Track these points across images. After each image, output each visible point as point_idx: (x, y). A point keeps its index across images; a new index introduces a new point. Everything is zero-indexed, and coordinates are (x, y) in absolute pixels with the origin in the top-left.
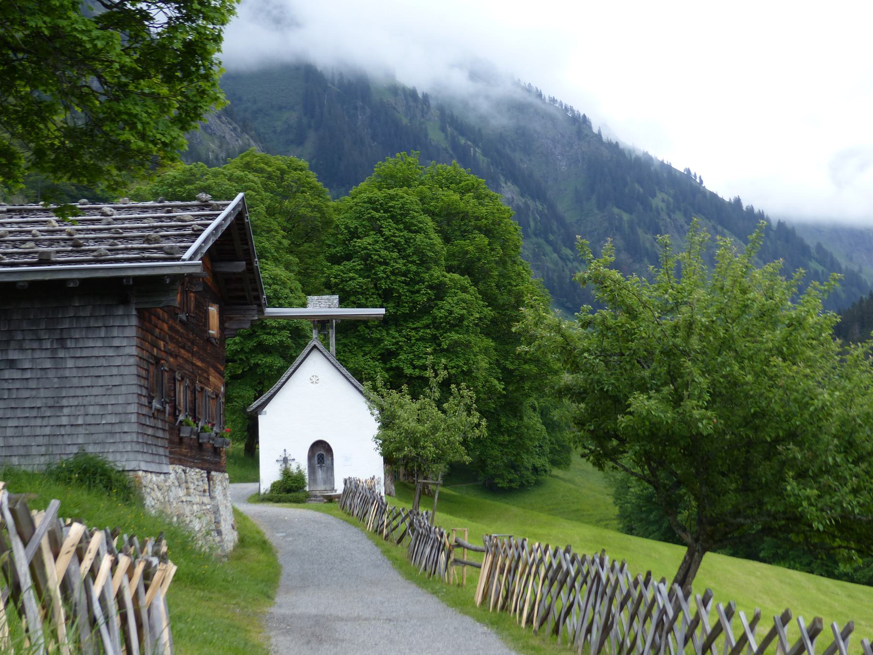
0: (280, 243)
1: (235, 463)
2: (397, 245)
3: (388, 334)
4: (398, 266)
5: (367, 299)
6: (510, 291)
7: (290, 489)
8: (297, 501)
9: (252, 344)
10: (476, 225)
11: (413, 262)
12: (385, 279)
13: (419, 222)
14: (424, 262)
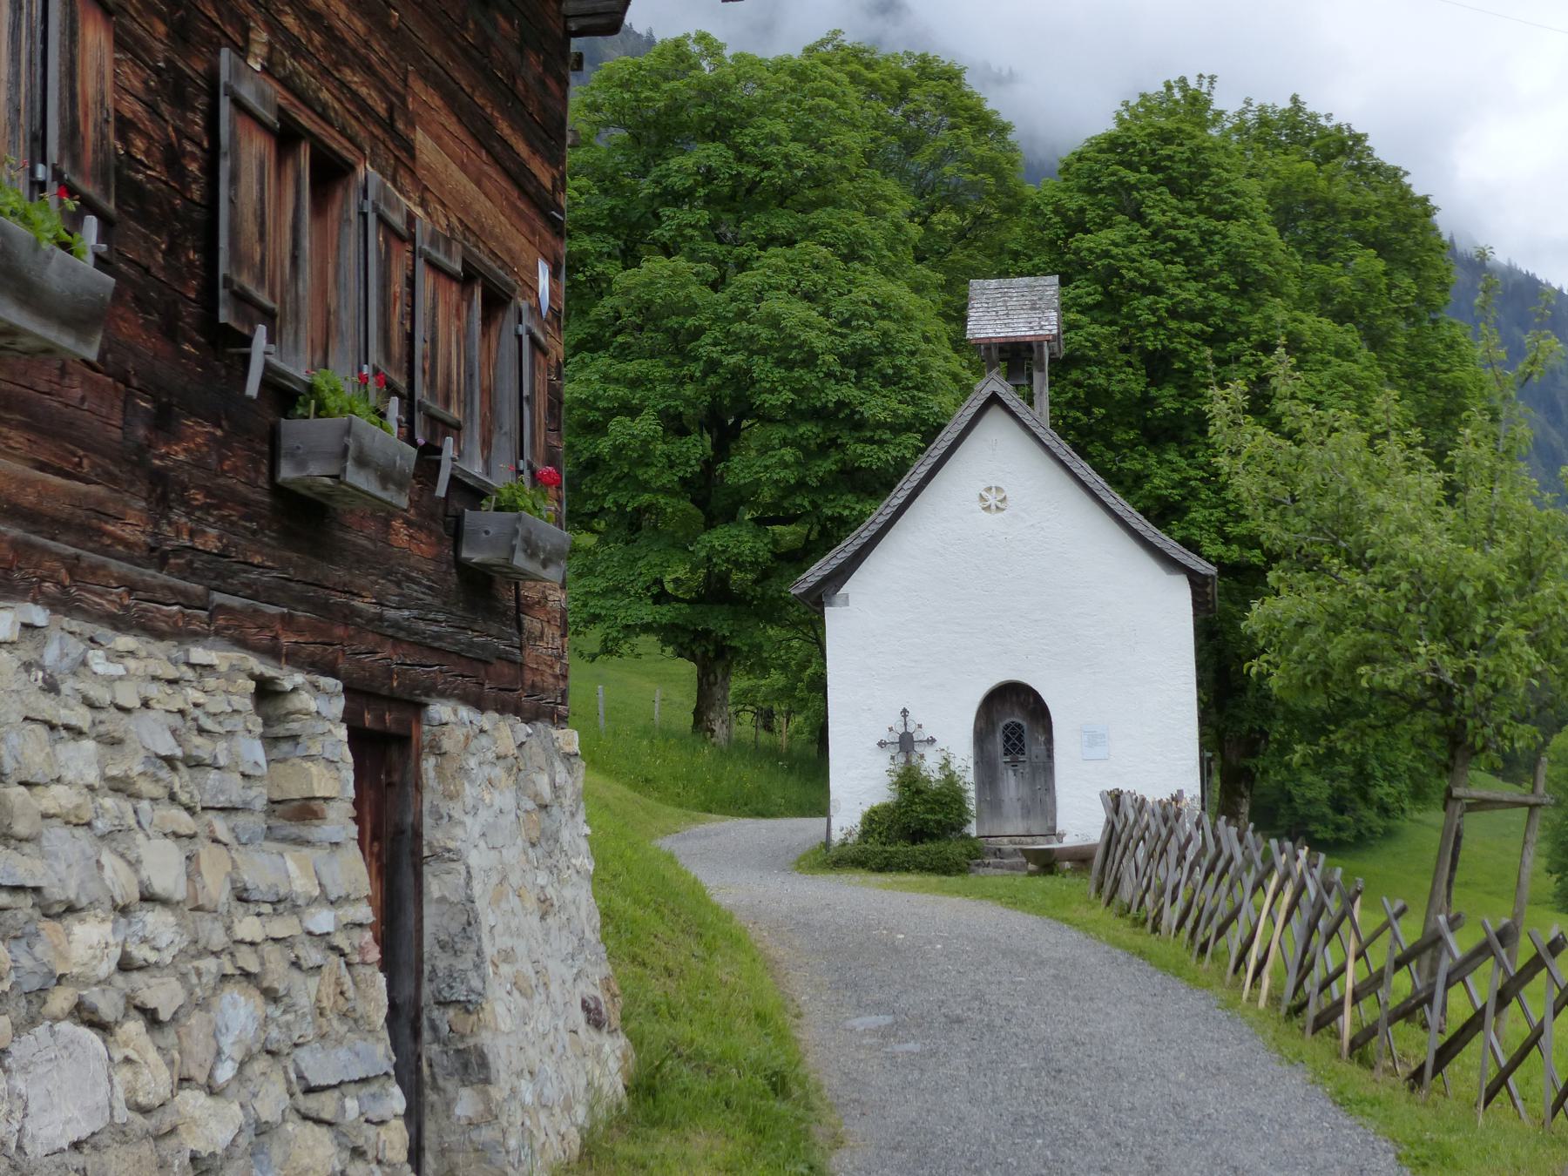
0: (899, 228)
1: (791, 769)
2: (1183, 245)
3: (1160, 462)
4: (1185, 295)
5: (1109, 375)
6: (1433, 385)
7: (920, 831)
8: (945, 867)
9: (828, 465)
10: (1353, 230)
11: (1222, 288)
12: (1154, 325)
13: (1234, 193)
14: (1249, 286)
